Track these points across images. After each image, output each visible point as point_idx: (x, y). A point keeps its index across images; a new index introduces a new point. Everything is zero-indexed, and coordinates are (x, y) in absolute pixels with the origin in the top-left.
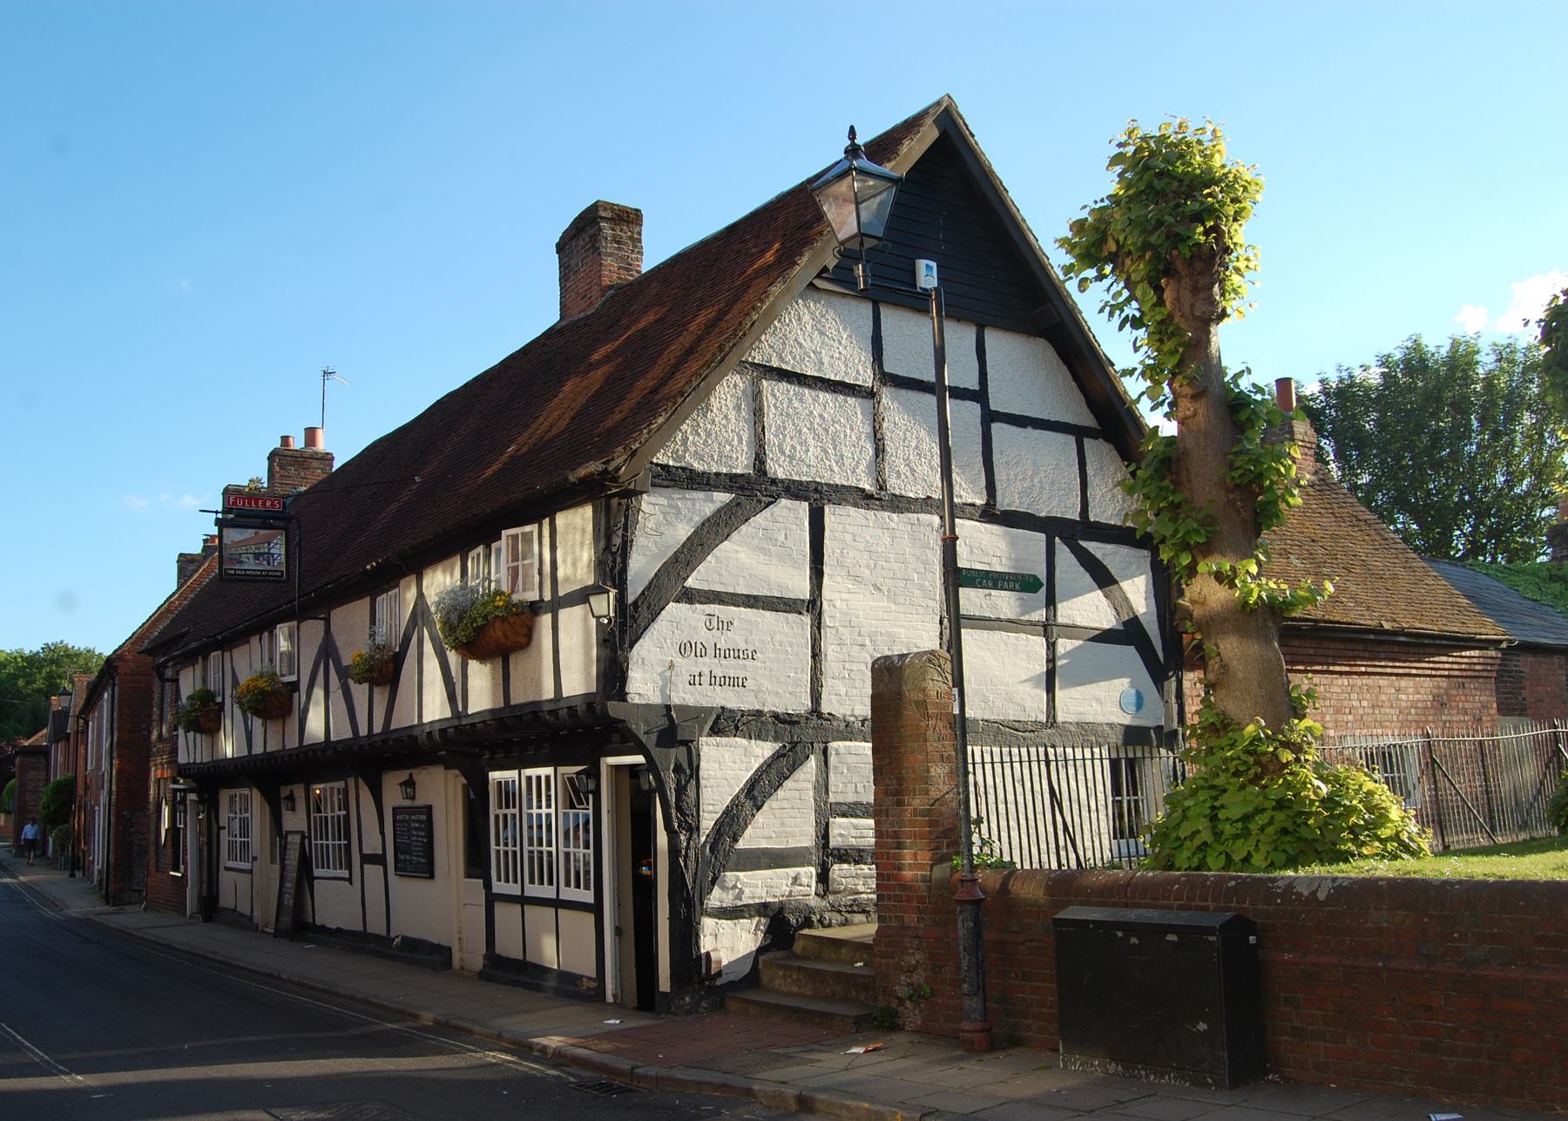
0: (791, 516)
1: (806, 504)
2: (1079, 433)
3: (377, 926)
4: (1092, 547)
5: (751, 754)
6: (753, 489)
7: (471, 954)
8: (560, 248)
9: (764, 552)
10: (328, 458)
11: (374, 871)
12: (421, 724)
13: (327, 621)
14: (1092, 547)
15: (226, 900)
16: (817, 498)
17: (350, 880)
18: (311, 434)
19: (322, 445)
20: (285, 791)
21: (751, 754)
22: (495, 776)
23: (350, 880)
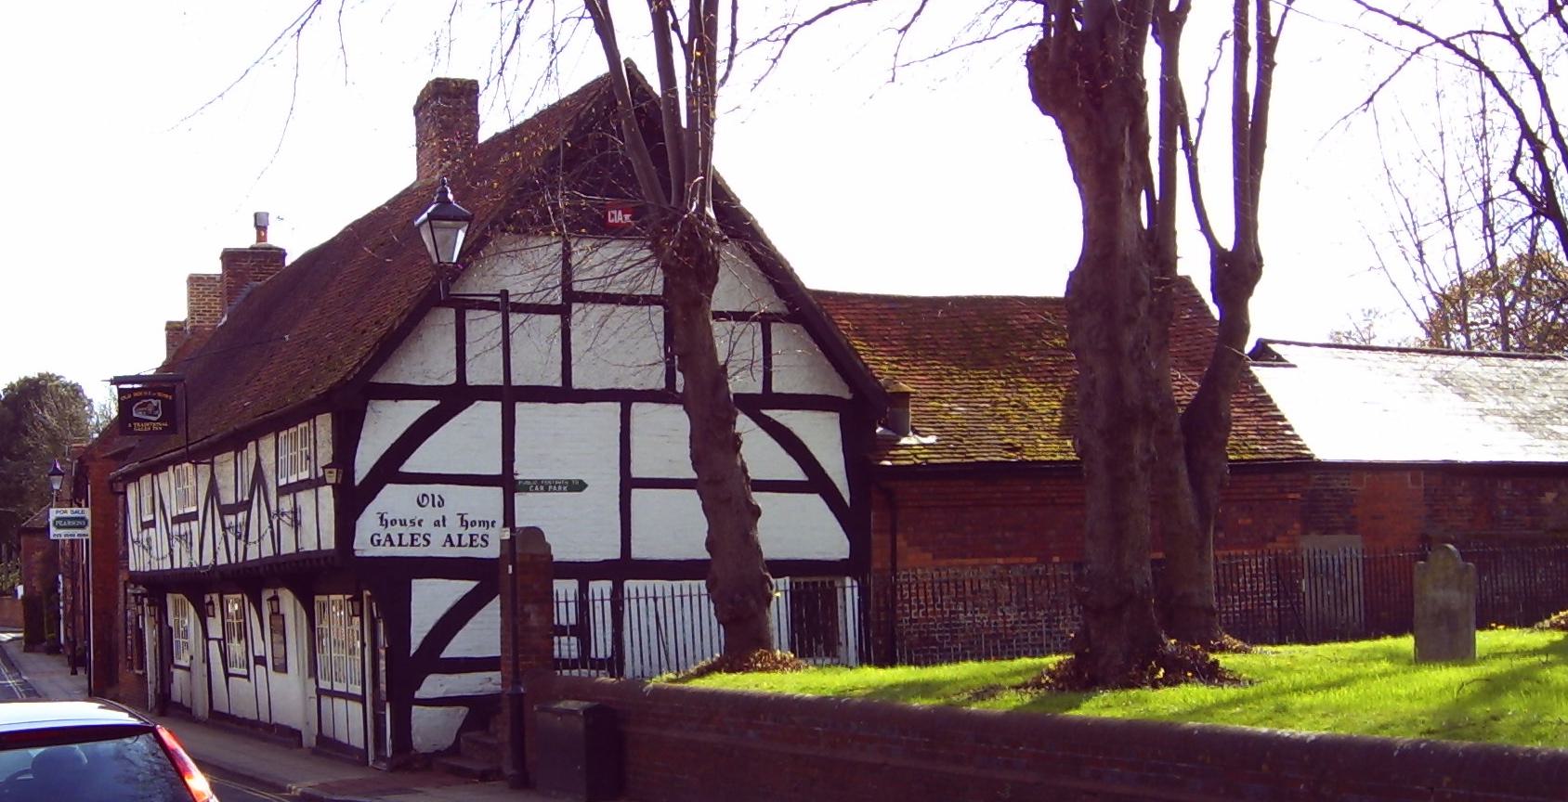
0: (486, 414)
1: (132, 568)
2: (766, 321)
3: (264, 717)
4: (774, 414)
5: (450, 591)
6: (454, 398)
7: (201, 709)
8: (417, 110)
9: (468, 440)
10: (281, 254)
11: (260, 669)
12: (277, 554)
13: (212, 464)
14: (774, 414)
15: (177, 692)
16: (509, 395)
17: (247, 677)
18: (261, 225)
19: (274, 239)
20: (207, 599)
21: (450, 591)
22: (317, 598)
23: (247, 677)
